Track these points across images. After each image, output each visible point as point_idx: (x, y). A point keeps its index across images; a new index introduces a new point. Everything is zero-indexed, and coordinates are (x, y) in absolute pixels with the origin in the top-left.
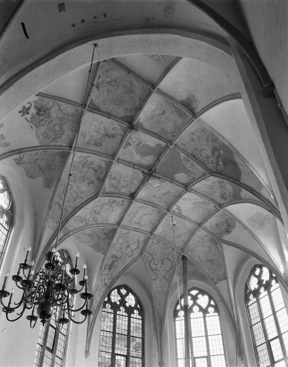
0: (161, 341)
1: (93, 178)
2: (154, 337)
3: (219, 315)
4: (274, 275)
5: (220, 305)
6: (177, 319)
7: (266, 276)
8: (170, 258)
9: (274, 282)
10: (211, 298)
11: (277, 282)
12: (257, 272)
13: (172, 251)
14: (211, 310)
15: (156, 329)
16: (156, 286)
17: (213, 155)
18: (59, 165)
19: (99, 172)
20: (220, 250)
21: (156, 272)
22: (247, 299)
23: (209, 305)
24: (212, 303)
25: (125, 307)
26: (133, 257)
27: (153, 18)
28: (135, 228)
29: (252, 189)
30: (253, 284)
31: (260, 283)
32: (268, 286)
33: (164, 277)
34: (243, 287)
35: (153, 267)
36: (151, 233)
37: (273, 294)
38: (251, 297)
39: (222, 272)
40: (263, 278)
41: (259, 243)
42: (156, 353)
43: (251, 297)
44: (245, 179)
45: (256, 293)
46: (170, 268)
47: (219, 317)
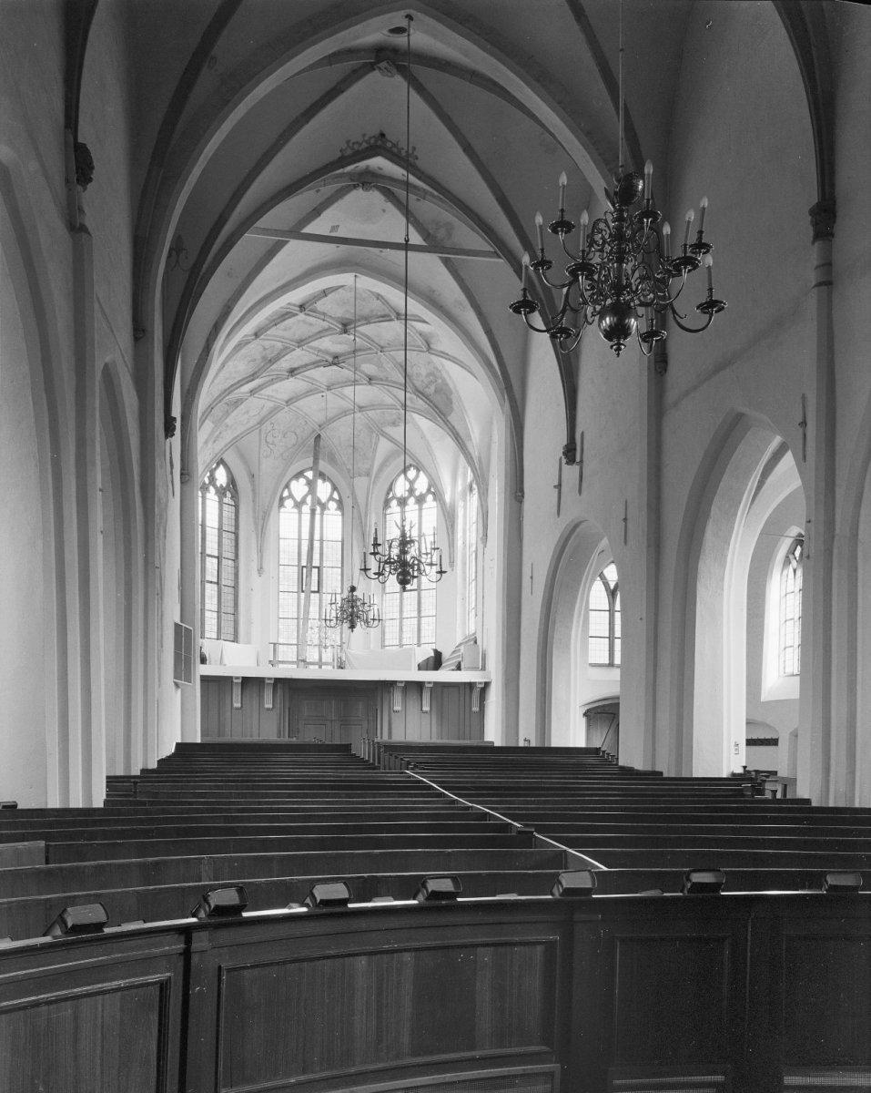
0: (262, 541)
1: (258, 357)
2: (254, 536)
3: (343, 515)
4: (432, 490)
5: (348, 503)
6: (282, 510)
7: (422, 485)
8: (298, 431)
9: (430, 497)
10: (335, 488)
11: (435, 499)
12: (412, 473)
13: (303, 423)
14: (332, 505)
15: (256, 524)
16: (268, 467)
17: (426, 377)
18: (432, 572)
19: (268, 352)
20: (374, 441)
21: (271, 446)
22: (387, 504)
23: (331, 498)
24: (336, 496)
25: (214, 486)
26: (248, 426)
27: (439, 295)
28: (268, 396)
29: (458, 434)
30: (401, 488)
31: (411, 491)
32: (420, 500)
33: (282, 454)
34: (387, 487)
35: (270, 439)
36: (287, 402)
37: (424, 512)
38: (394, 503)
39: (367, 466)
40: (416, 486)
41: (431, 453)
42: (255, 556)
43: (394, 503)
44: (452, 418)
45: (402, 502)
46: (83, 229)
47: (343, 518)
